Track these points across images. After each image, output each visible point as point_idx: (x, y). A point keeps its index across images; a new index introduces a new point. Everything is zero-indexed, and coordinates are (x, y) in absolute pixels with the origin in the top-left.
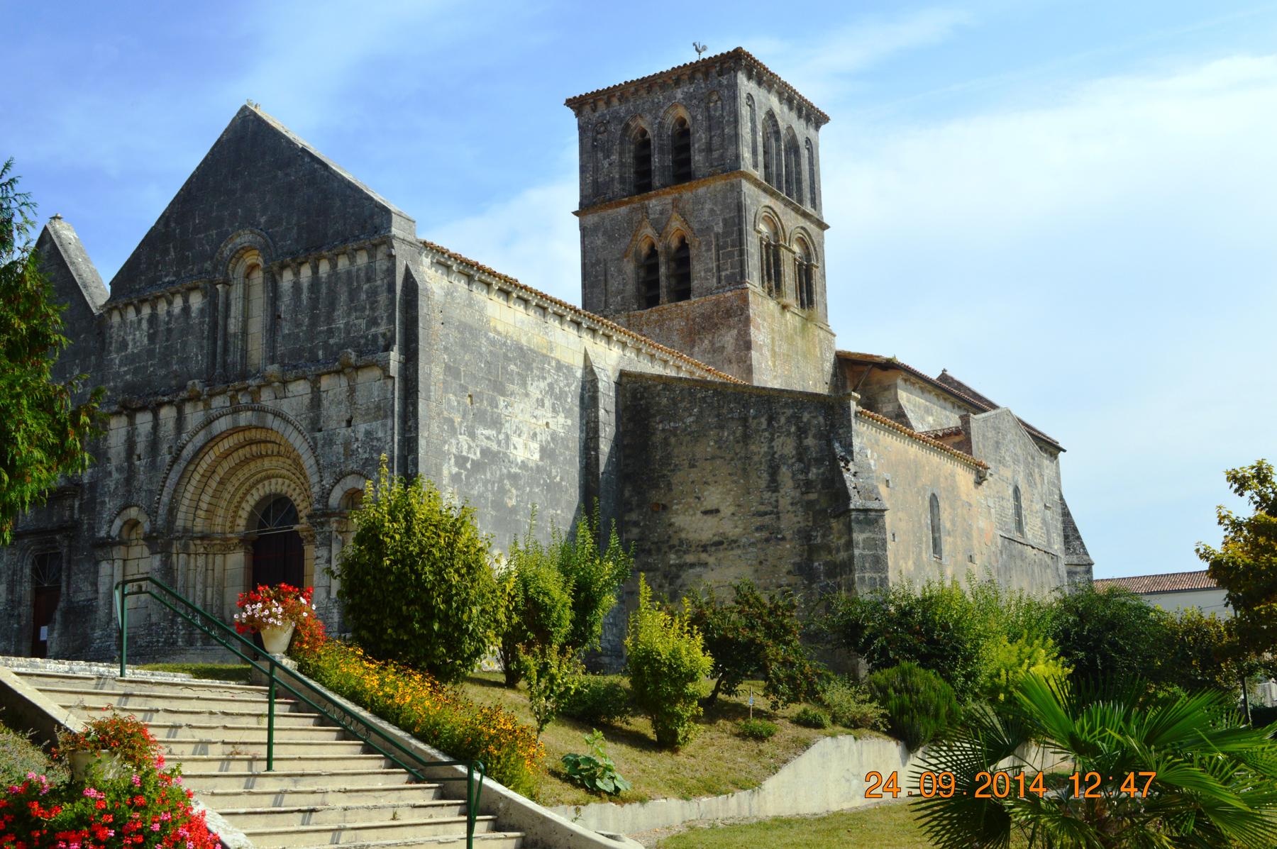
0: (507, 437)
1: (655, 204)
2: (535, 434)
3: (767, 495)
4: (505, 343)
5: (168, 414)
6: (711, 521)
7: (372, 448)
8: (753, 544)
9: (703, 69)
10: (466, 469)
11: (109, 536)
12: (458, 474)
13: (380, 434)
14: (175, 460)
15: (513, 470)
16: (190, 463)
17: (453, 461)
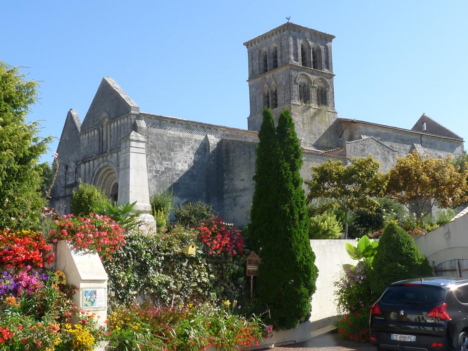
1: (268, 76)
2: (186, 162)
4: (174, 137)
5: (91, 162)
9: (279, 30)
10: (159, 174)
12: (156, 176)
14: (93, 175)
15: (177, 173)
16: (96, 175)
17: (154, 172)
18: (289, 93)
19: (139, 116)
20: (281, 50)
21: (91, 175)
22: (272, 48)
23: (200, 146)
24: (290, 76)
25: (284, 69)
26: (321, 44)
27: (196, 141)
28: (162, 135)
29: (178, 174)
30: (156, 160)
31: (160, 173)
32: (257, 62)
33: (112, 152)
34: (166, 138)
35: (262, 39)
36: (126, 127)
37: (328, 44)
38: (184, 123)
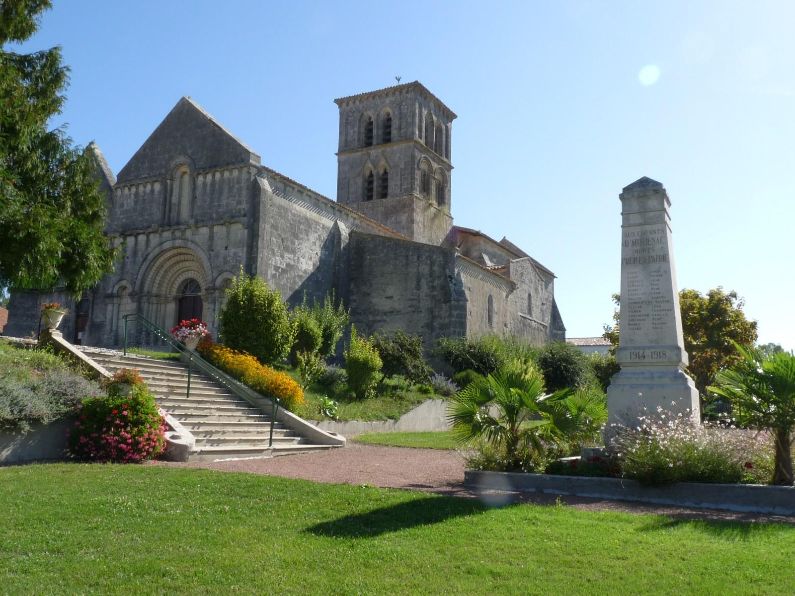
0: (298, 259)
1: (374, 152)
2: (311, 258)
5: (142, 238)
6: (389, 302)
7: (237, 260)
8: (407, 313)
11: (112, 293)
12: (275, 274)
13: (241, 254)
14: (144, 260)
17: (273, 268)
18: (409, 180)
19: (263, 171)
20: (400, 118)
21: (140, 258)
22: (383, 114)
23: (328, 236)
24: (413, 157)
25: (403, 145)
26: (443, 123)
27: (324, 227)
28: (286, 210)
29: (300, 277)
30: (276, 250)
32: (356, 129)
33: (200, 224)
34: (290, 217)
35: (368, 98)
36: (237, 186)
37: (449, 125)
38: (313, 196)
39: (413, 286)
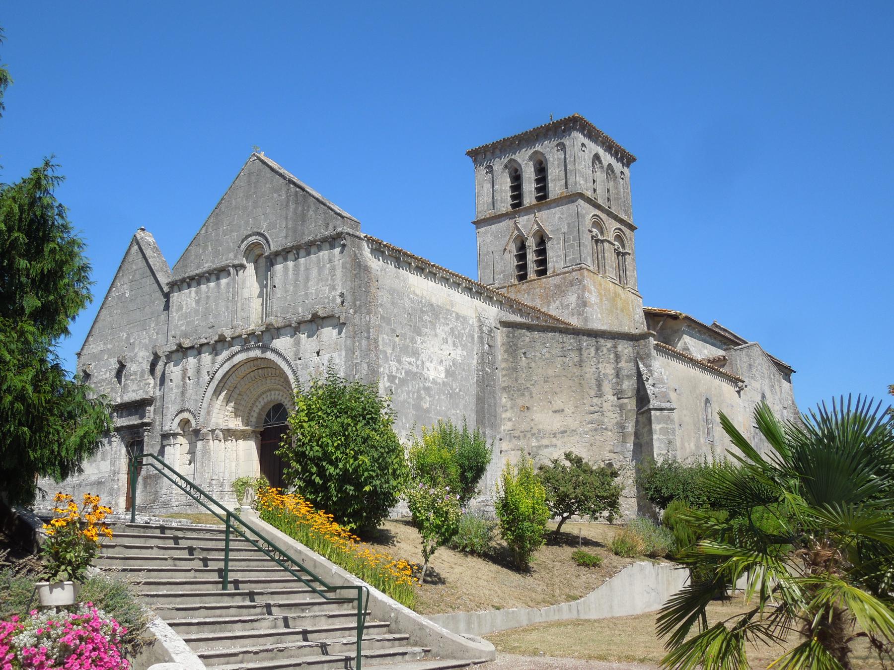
0: (423, 363)
2: (442, 361)
3: (595, 400)
8: (585, 433)
17: (386, 378)
31: (397, 381)
39: (593, 393)
